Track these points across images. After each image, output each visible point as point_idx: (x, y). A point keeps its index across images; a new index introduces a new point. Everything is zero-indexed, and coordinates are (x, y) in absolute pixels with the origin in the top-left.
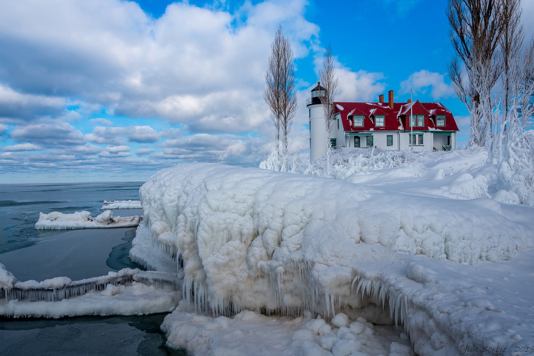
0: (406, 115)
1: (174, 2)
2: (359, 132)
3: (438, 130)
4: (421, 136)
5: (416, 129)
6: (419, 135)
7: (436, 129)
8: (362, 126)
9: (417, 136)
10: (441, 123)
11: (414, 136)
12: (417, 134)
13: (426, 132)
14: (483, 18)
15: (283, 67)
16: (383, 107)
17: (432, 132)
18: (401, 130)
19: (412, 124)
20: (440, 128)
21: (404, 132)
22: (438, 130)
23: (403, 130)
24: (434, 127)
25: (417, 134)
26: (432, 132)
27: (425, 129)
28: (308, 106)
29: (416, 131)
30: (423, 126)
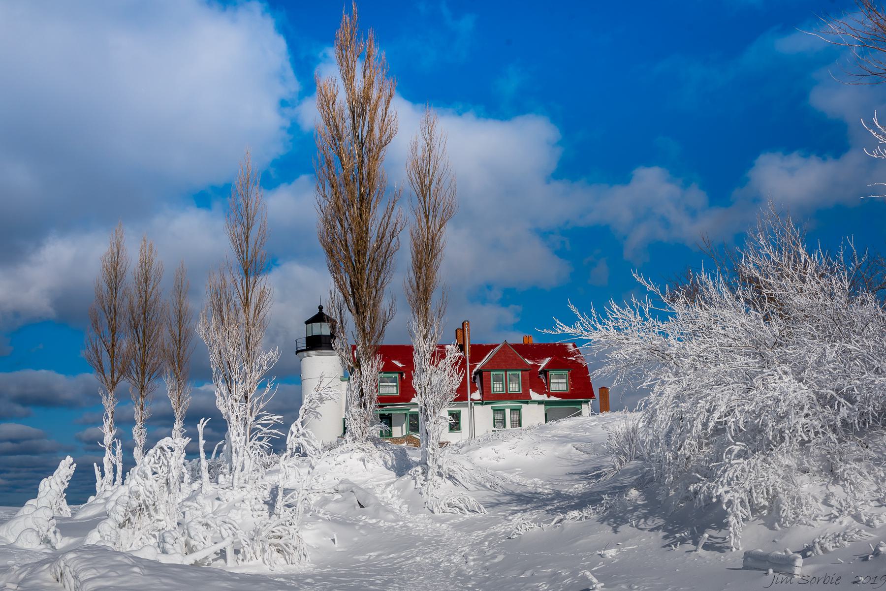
0: (483, 370)
1: (283, 128)
2: (386, 406)
3: (553, 398)
4: (518, 410)
5: (507, 396)
6: (511, 410)
7: (549, 397)
8: (395, 392)
9: (508, 411)
10: (559, 383)
11: (502, 411)
12: (508, 407)
13: (527, 403)
14: (429, 212)
15: (384, 250)
16: (265, 394)
17: (540, 403)
18: (475, 400)
19: (497, 388)
20: (557, 395)
21: (482, 404)
22: (553, 398)
23: (479, 400)
24: (546, 392)
25: (508, 407)
26: (540, 403)
27: (524, 398)
28: (299, 354)
29: (506, 402)
30: (519, 391)
